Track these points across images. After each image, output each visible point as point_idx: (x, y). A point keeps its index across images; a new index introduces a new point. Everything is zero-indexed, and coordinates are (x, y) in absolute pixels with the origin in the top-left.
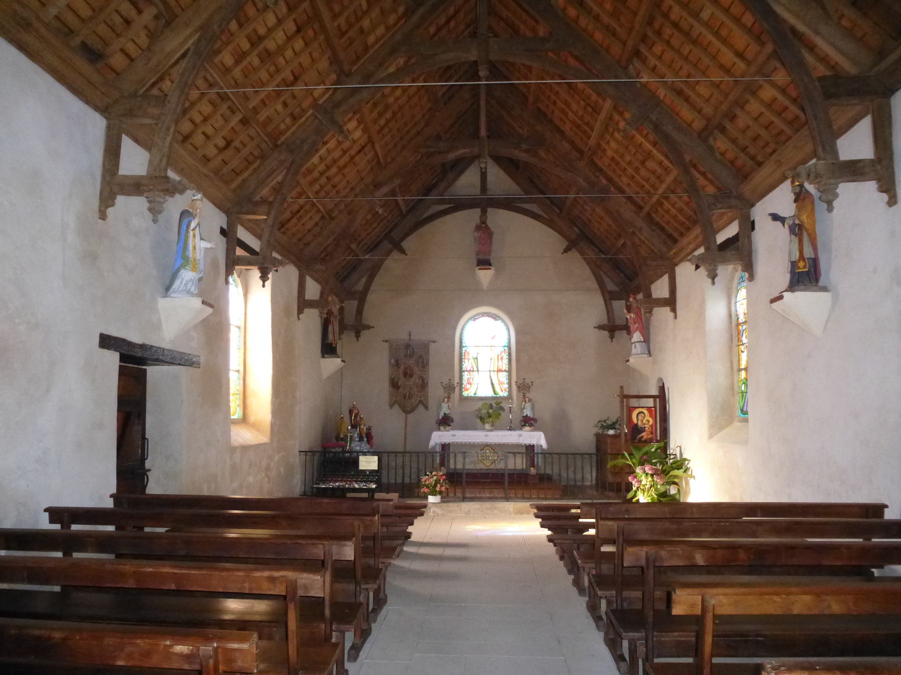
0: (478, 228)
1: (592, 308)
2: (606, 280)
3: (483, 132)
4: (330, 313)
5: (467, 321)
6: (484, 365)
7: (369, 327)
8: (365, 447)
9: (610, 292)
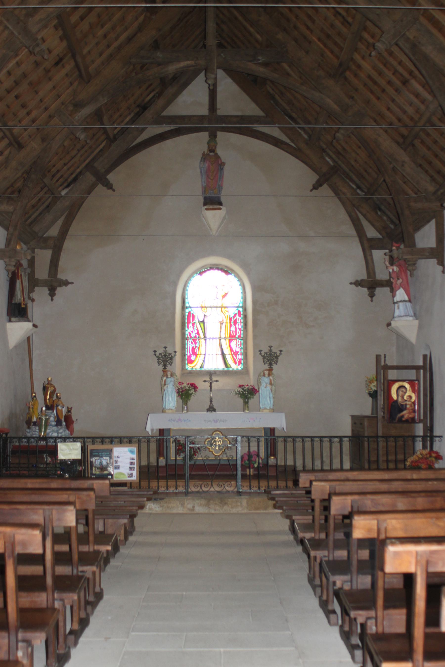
0: (205, 157)
1: (347, 261)
2: (365, 223)
3: (212, 41)
4: (19, 265)
5: (191, 276)
6: (213, 329)
7: (66, 283)
8: (63, 432)
9: (371, 240)
